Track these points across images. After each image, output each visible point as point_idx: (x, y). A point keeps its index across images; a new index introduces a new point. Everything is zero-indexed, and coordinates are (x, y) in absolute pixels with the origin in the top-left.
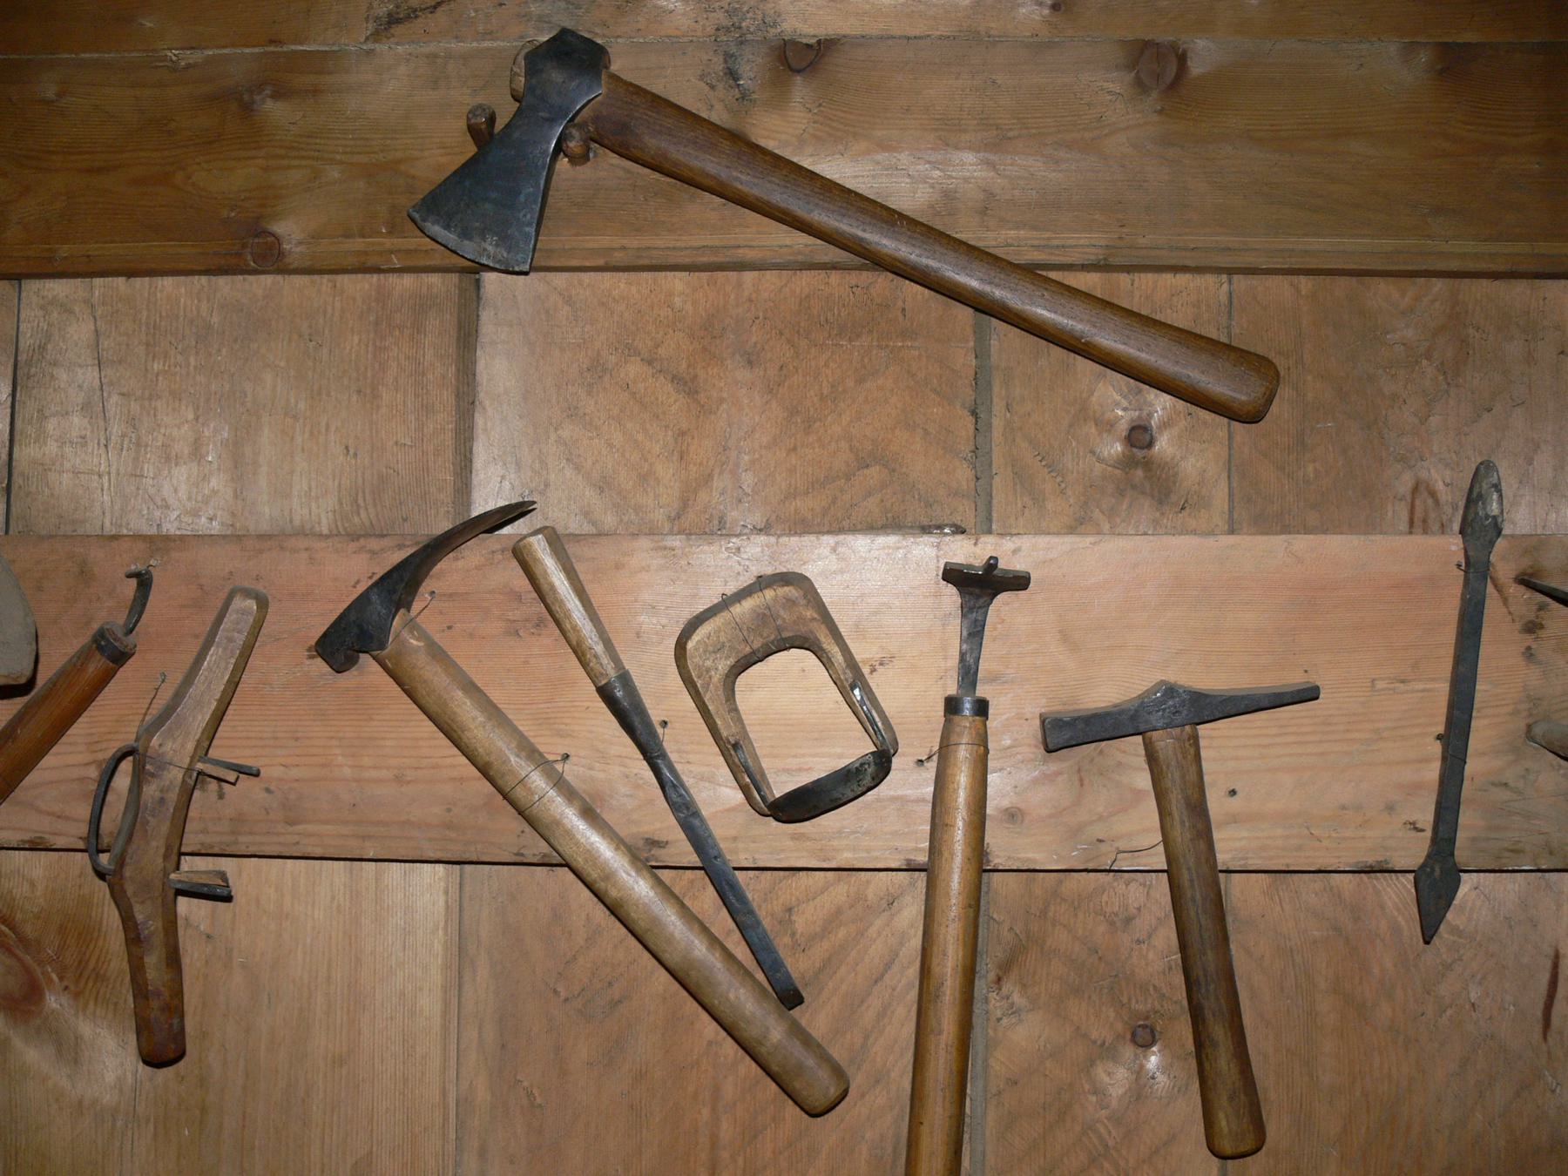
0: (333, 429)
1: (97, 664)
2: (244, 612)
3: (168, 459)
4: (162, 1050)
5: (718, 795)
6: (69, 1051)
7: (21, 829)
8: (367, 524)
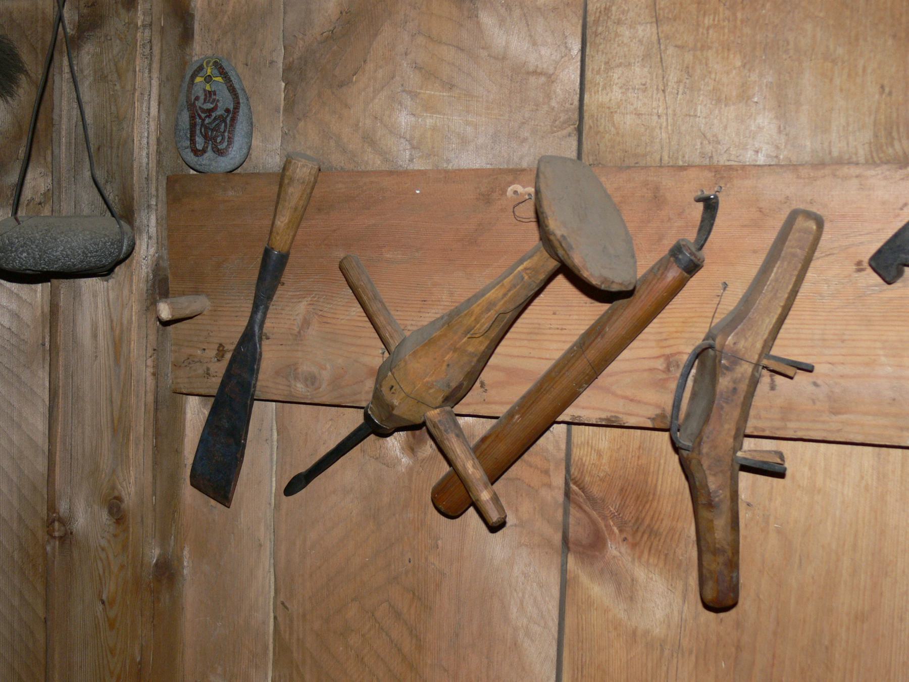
0: (869, 71)
1: (673, 273)
2: (806, 231)
3: (719, 100)
4: (720, 599)
6: (627, 590)
7: (599, 409)
8: (901, 154)
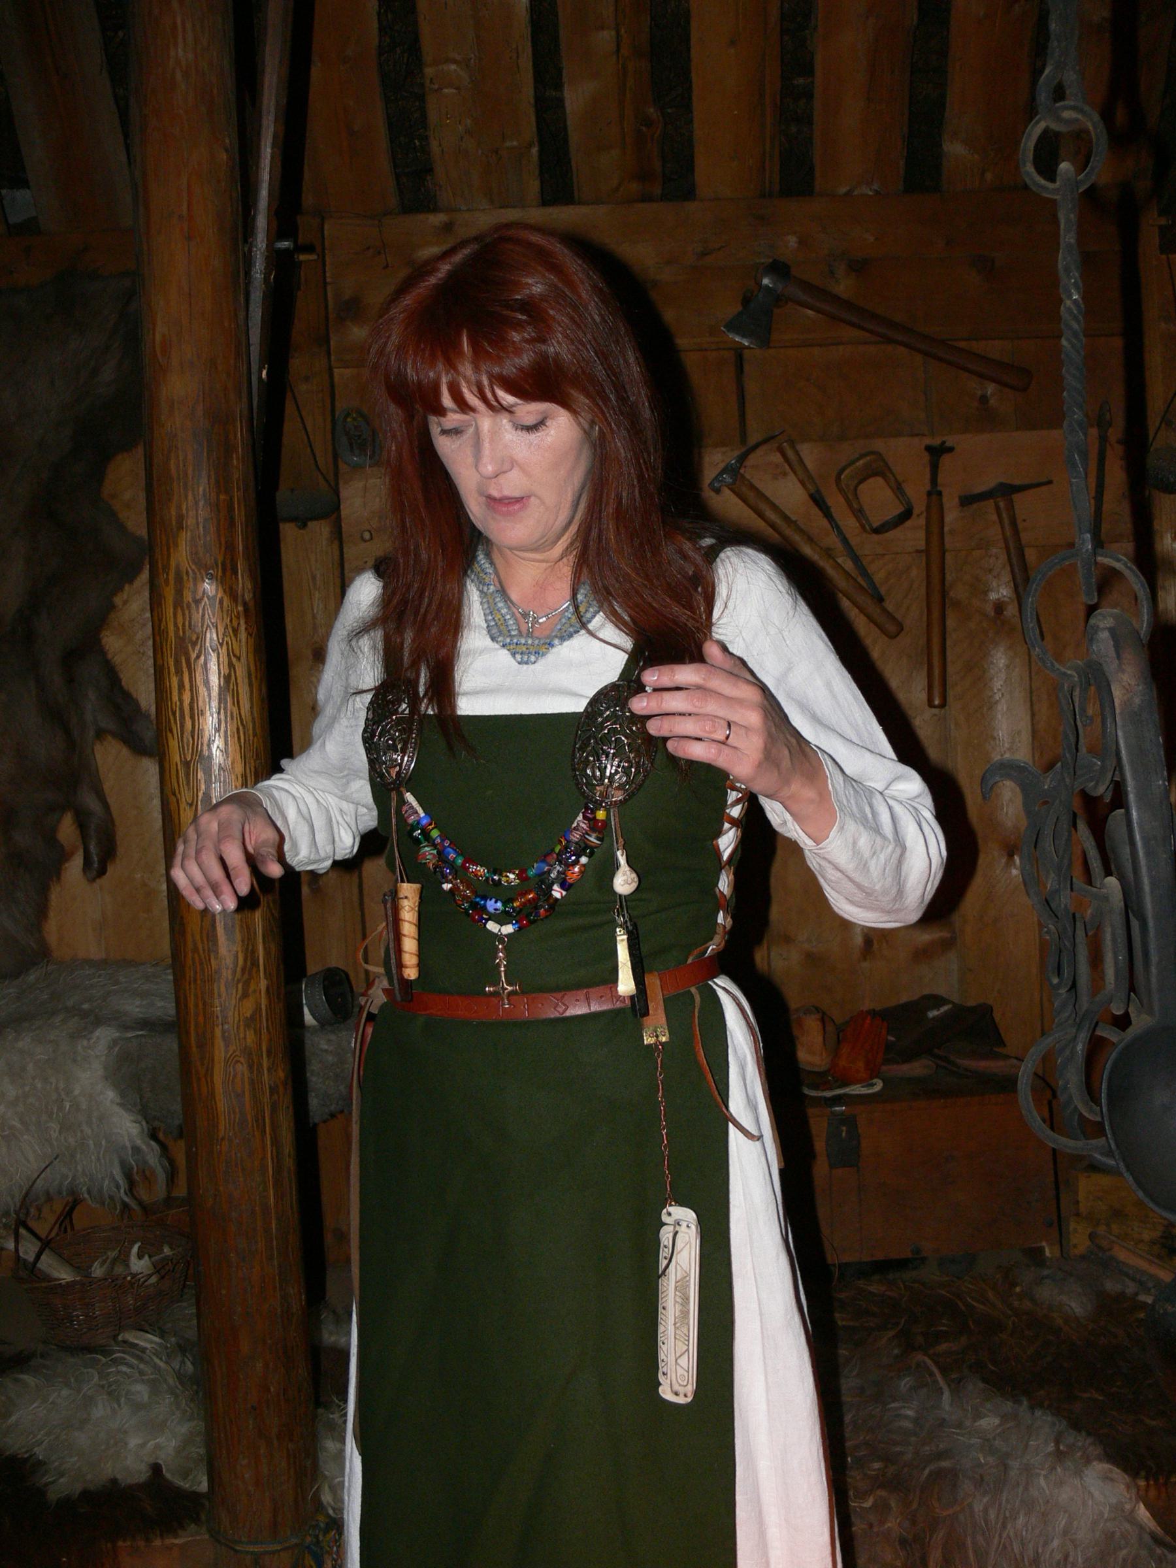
5: (849, 523)
